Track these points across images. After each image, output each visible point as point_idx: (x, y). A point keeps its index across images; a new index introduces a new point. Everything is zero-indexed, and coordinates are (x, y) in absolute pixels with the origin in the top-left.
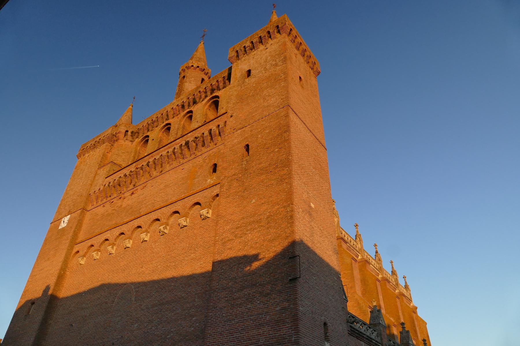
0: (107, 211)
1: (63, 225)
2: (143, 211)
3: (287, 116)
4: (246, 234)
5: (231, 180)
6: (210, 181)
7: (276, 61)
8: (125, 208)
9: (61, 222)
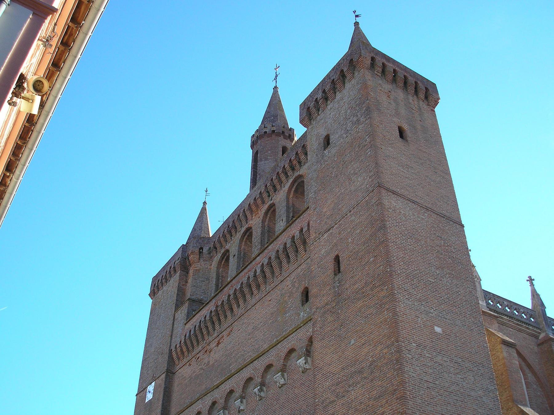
0: (194, 372)
1: (149, 396)
2: (234, 367)
3: (380, 204)
4: (348, 391)
5: (325, 313)
6: (303, 315)
7: (357, 116)
8: (213, 364)
9: (146, 392)
